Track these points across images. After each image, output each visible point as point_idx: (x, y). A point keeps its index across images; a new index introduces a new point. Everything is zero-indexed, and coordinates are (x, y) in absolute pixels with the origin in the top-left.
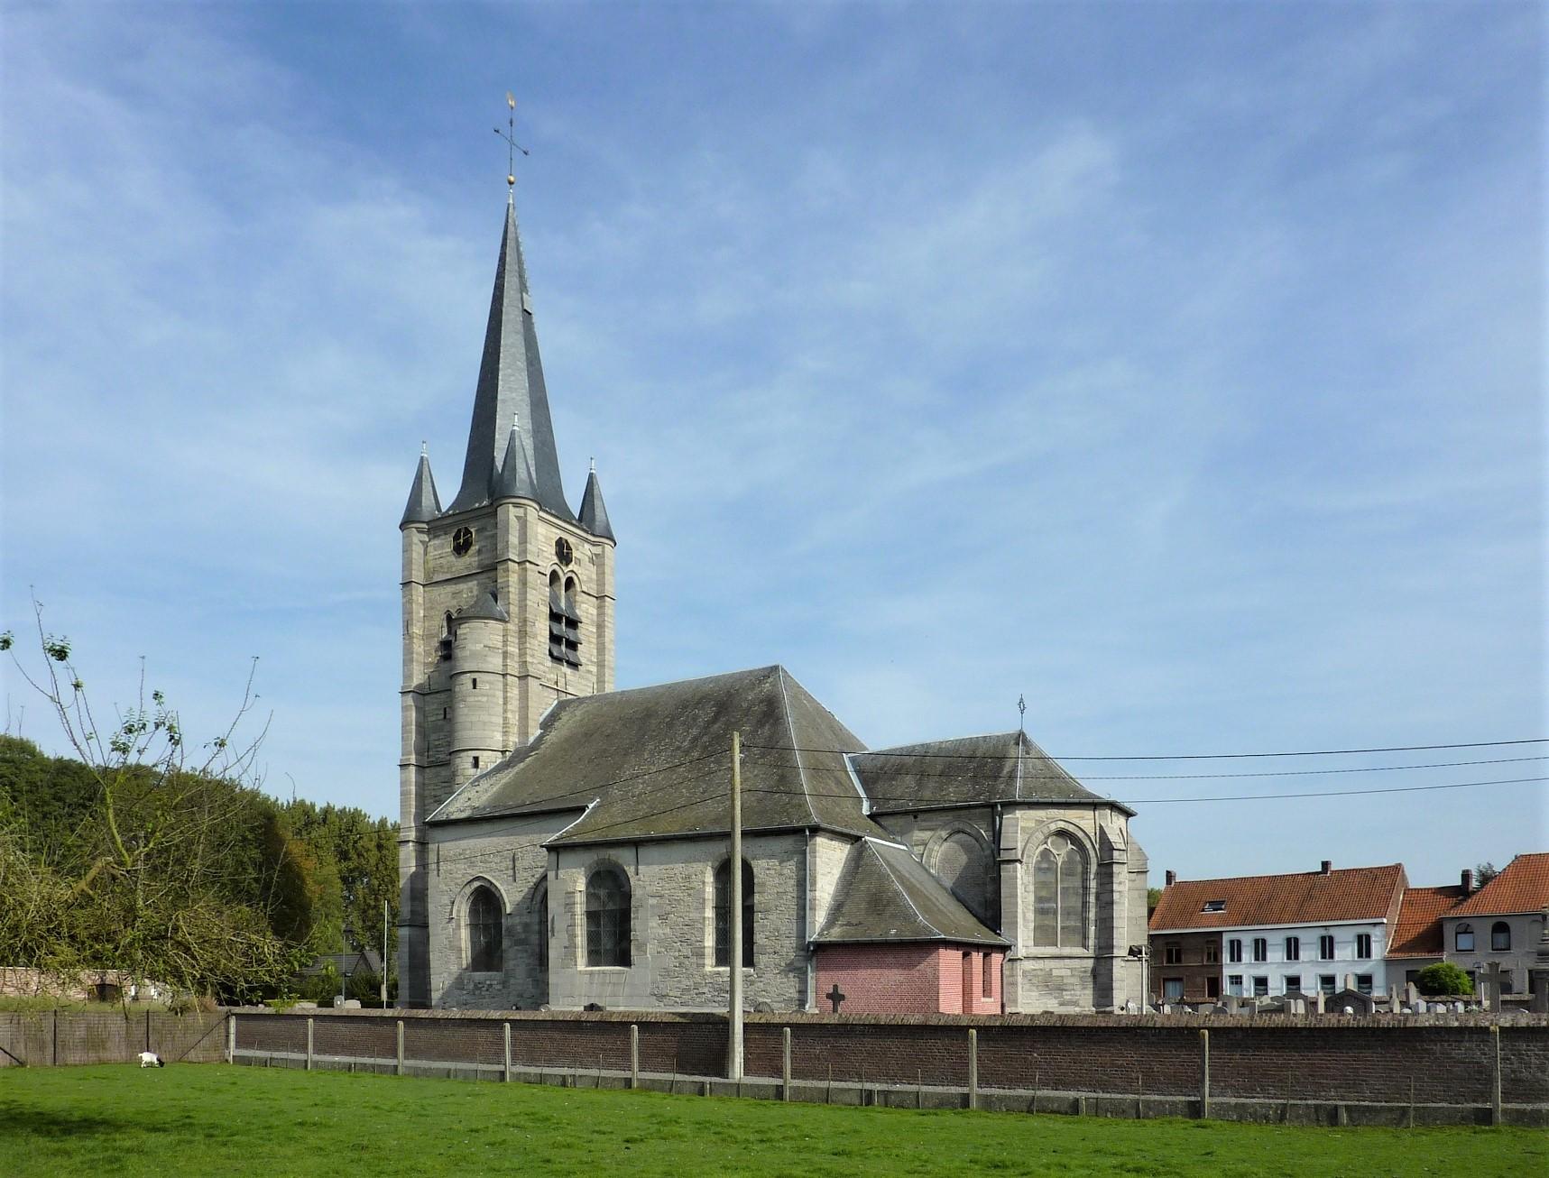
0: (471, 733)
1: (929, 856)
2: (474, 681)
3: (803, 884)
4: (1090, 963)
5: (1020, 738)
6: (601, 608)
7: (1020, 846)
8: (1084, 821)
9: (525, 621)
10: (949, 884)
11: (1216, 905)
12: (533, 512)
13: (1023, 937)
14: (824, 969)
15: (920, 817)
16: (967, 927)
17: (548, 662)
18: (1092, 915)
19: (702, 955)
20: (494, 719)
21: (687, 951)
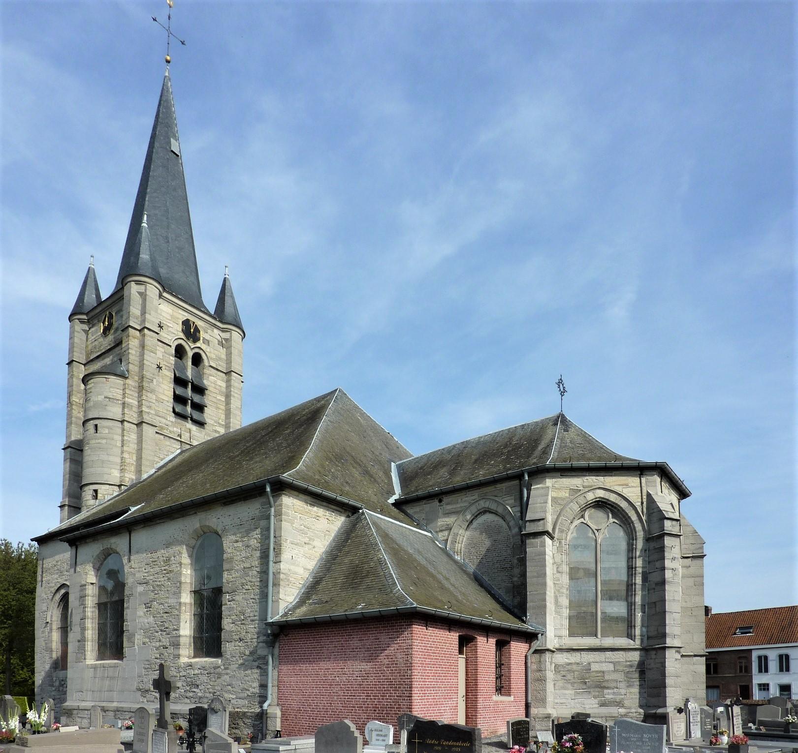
0: (92, 470)
1: (454, 542)
2: (96, 426)
3: (267, 554)
4: (635, 656)
5: (561, 420)
6: (228, 381)
7: (550, 519)
8: (630, 489)
9: (142, 378)
10: (471, 568)
11: (745, 630)
12: (153, 289)
13: (555, 628)
14: (288, 662)
15: (446, 500)
16: (481, 608)
17: (172, 418)
18: (638, 599)
19: (176, 645)
20: (111, 458)
21: (166, 641)
